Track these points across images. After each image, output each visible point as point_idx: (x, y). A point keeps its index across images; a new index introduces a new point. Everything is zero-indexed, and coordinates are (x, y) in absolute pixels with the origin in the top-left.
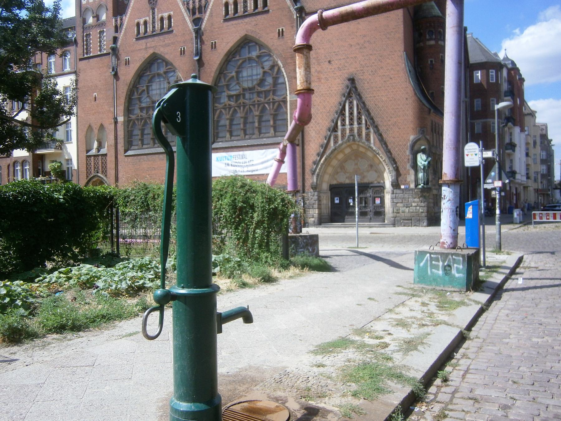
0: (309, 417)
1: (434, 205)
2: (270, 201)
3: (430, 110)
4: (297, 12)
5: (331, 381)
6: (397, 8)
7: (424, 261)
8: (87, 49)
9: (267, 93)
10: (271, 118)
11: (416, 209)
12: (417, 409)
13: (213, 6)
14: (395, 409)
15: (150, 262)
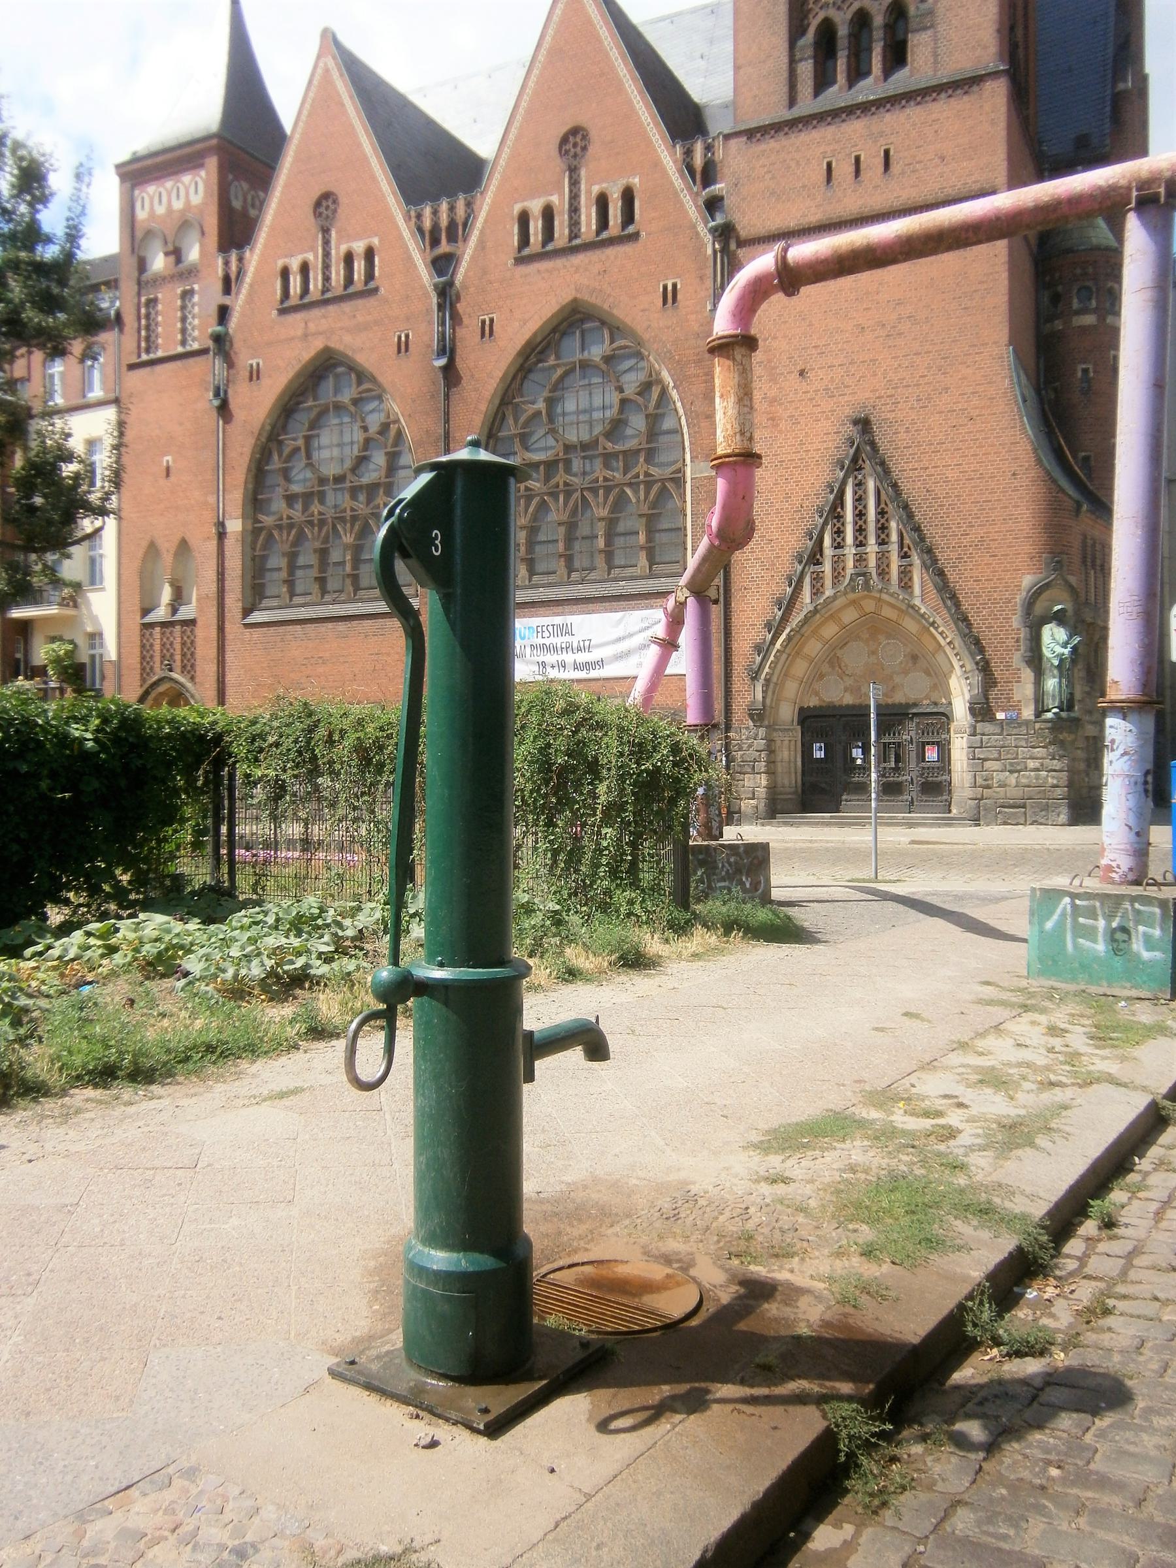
0: (751, 1302)
1: (1089, 766)
2: (641, 752)
3: (1079, 505)
4: (714, 237)
5: (806, 1217)
6: (990, 239)
7: (1055, 917)
8: (148, 339)
9: (630, 456)
10: (640, 526)
11: (1037, 778)
12: (1031, 1294)
13: (486, 221)
14: (973, 1290)
15: (322, 910)
